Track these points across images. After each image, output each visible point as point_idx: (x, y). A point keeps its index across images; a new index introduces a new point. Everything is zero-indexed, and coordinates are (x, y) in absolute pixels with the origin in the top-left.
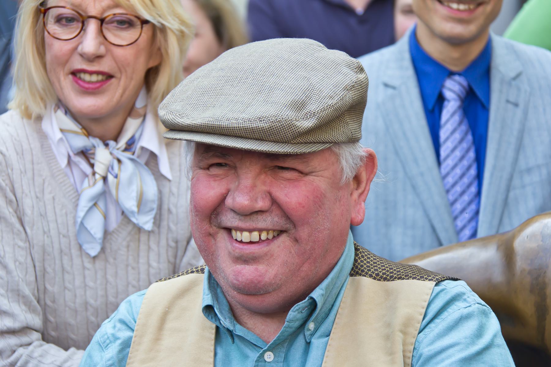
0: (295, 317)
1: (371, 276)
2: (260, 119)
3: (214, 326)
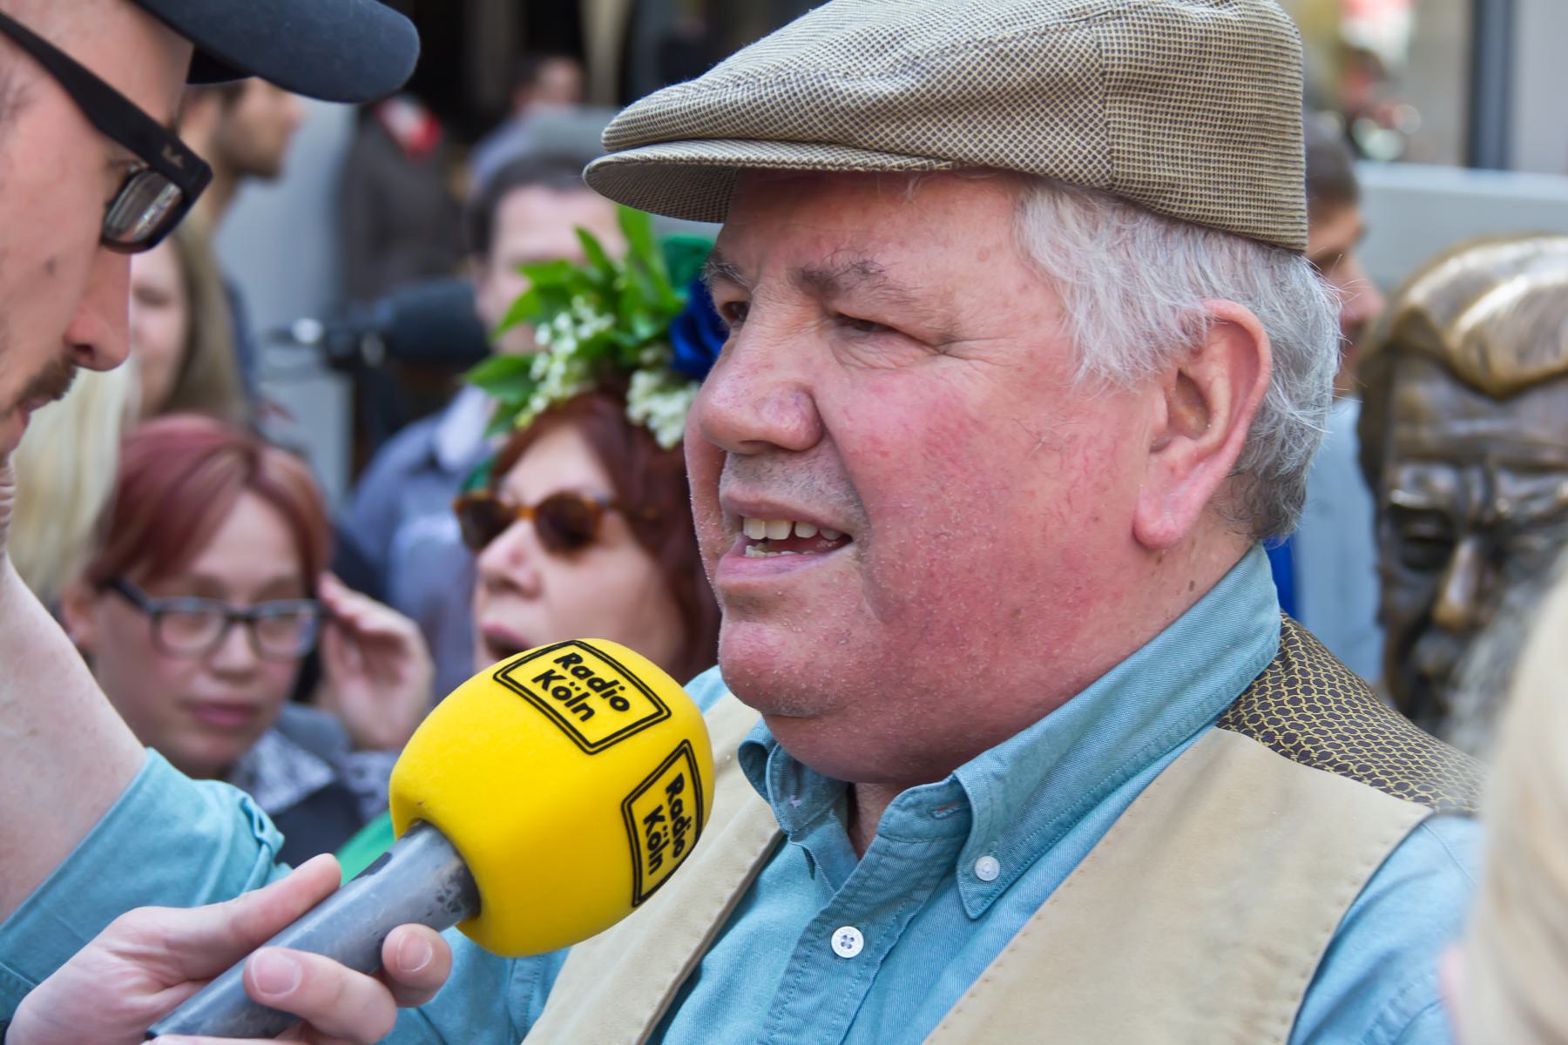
0: (904, 825)
1: (1269, 738)
3: (772, 832)
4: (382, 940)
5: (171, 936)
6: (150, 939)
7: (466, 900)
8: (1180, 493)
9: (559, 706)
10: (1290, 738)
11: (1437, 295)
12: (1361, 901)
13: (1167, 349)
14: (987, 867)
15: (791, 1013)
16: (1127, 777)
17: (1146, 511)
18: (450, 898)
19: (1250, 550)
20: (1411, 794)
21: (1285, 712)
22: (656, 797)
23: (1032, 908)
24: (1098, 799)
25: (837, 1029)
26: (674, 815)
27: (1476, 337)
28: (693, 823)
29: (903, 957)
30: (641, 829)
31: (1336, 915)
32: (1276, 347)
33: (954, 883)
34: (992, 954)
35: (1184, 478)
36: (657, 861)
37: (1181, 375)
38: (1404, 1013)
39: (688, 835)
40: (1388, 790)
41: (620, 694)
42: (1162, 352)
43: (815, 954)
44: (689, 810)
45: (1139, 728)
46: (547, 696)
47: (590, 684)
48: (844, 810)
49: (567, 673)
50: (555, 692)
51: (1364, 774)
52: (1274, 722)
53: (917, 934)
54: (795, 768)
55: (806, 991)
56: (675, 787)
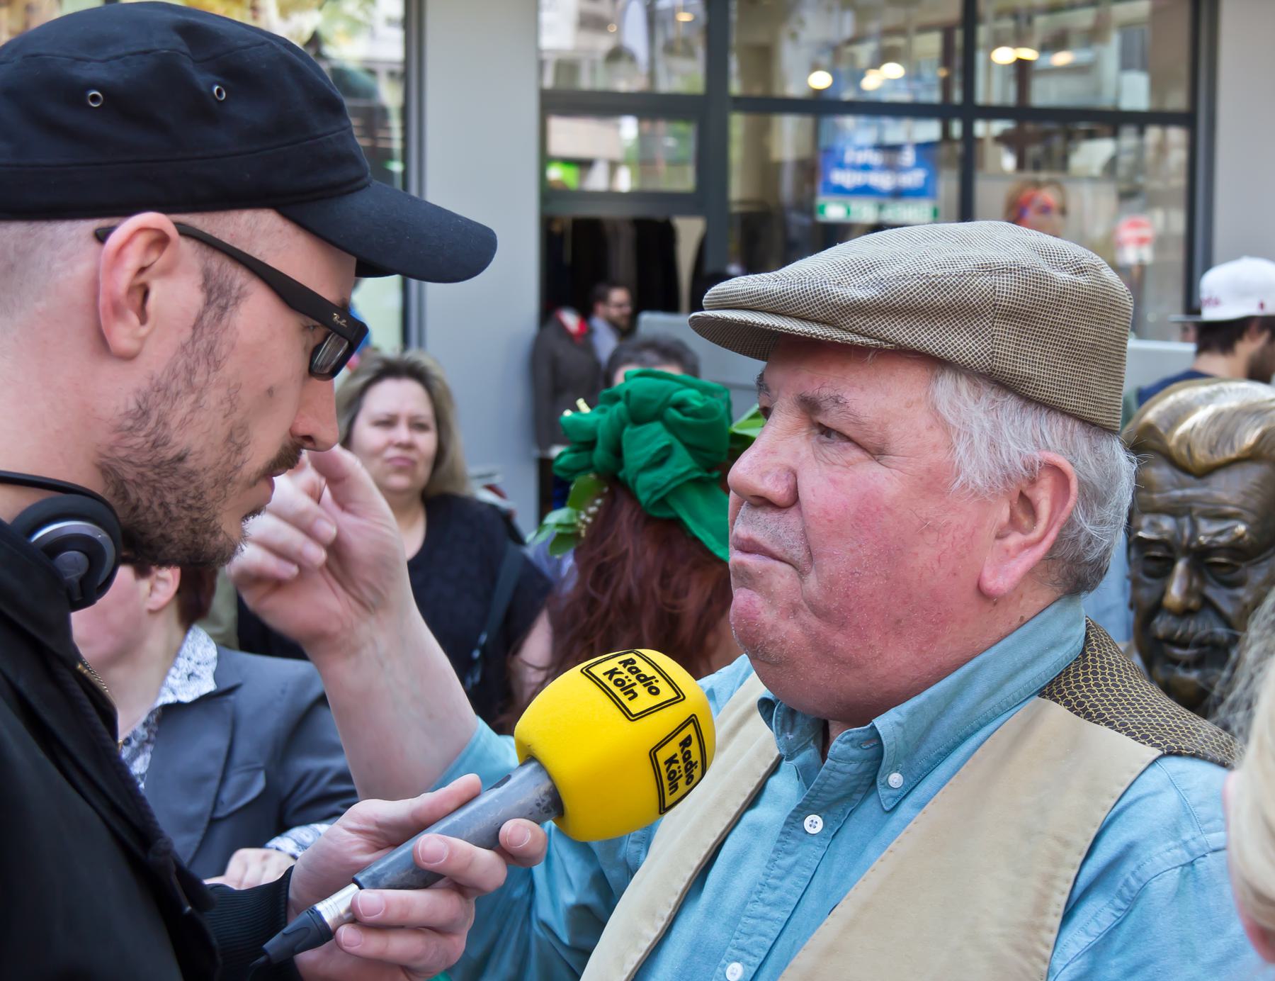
0: (844, 752)
1: (1068, 703)
2: (988, 269)
3: (777, 753)
4: (497, 833)
5: (378, 819)
6: (367, 821)
7: (553, 805)
8: (1008, 566)
9: (616, 690)
10: (1080, 704)
11: (1162, 416)
12: (1116, 809)
13: (1013, 476)
14: (896, 779)
15: (779, 867)
16: (982, 726)
17: (987, 573)
18: (544, 804)
19: (1059, 599)
20: (1150, 741)
21: (1079, 687)
22: (673, 748)
23: (921, 806)
24: (963, 739)
25: (805, 877)
26: (685, 760)
27: (1183, 439)
28: (699, 765)
29: (846, 833)
30: (663, 768)
31: (1101, 816)
32: (1081, 483)
33: (876, 789)
34: (895, 834)
35: (1014, 557)
36: (674, 787)
37: (1022, 495)
38: (1139, 880)
39: (696, 773)
40: (1136, 739)
41: (655, 684)
42: (1010, 478)
43: (794, 831)
44: (695, 756)
45: (987, 696)
46: (610, 684)
47: (638, 678)
48: (820, 741)
49: (625, 671)
50: (615, 683)
51: (1124, 729)
52: (1072, 693)
53: (853, 820)
54: (791, 713)
55: (788, 853)
56: (686, 743)
